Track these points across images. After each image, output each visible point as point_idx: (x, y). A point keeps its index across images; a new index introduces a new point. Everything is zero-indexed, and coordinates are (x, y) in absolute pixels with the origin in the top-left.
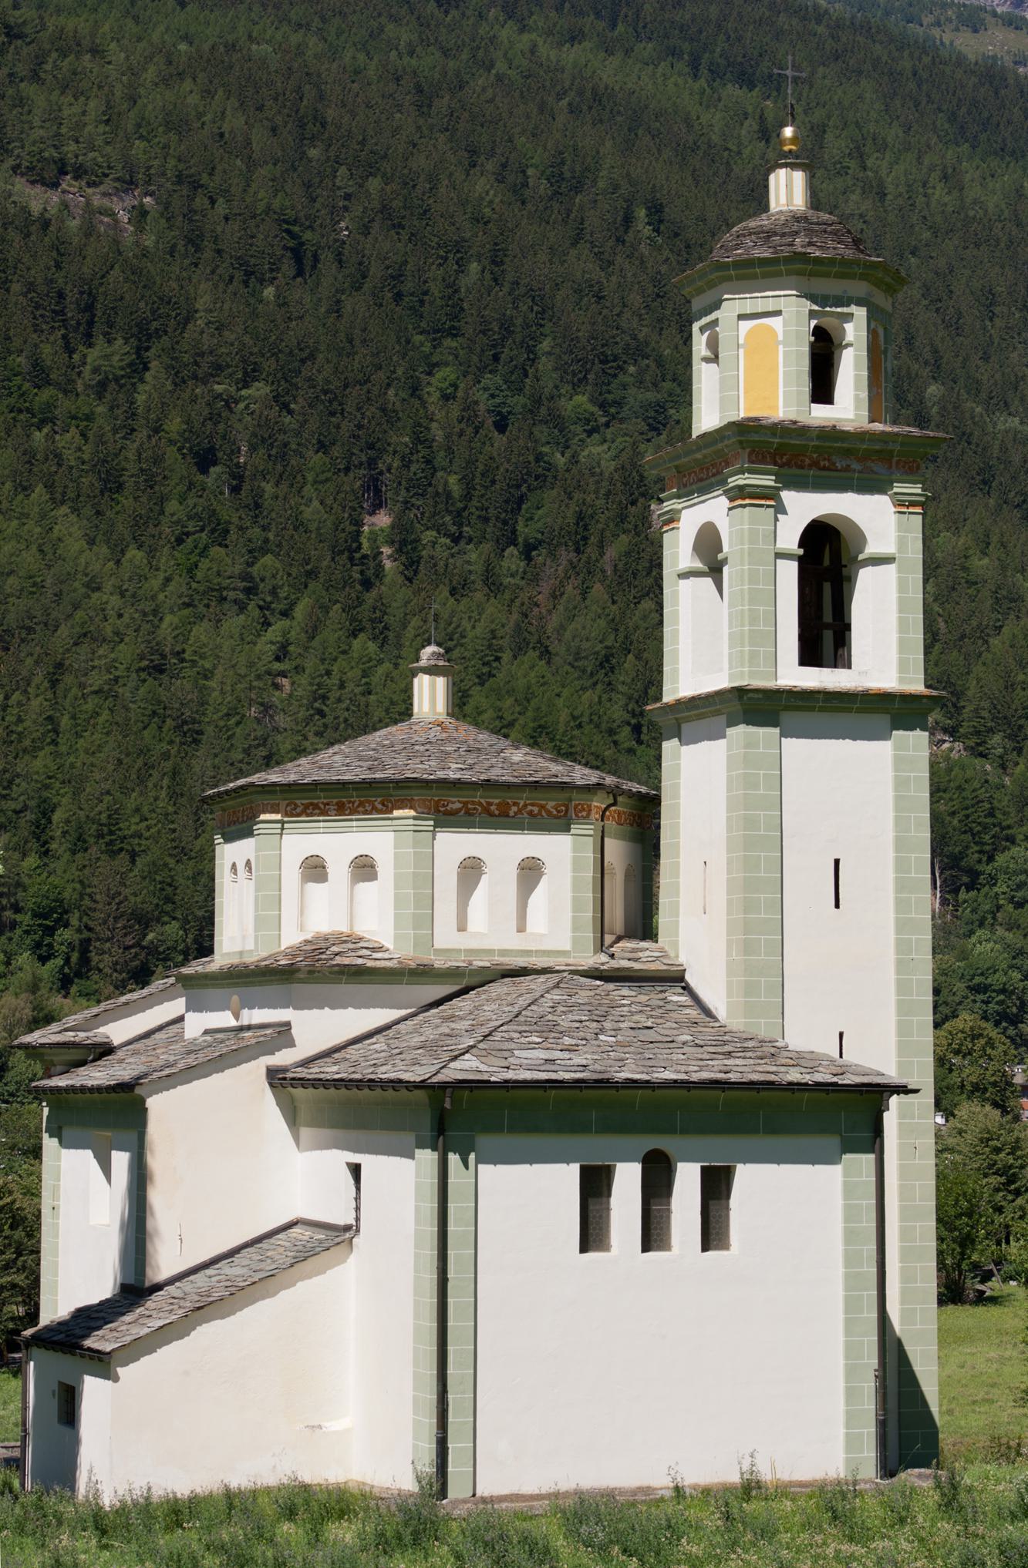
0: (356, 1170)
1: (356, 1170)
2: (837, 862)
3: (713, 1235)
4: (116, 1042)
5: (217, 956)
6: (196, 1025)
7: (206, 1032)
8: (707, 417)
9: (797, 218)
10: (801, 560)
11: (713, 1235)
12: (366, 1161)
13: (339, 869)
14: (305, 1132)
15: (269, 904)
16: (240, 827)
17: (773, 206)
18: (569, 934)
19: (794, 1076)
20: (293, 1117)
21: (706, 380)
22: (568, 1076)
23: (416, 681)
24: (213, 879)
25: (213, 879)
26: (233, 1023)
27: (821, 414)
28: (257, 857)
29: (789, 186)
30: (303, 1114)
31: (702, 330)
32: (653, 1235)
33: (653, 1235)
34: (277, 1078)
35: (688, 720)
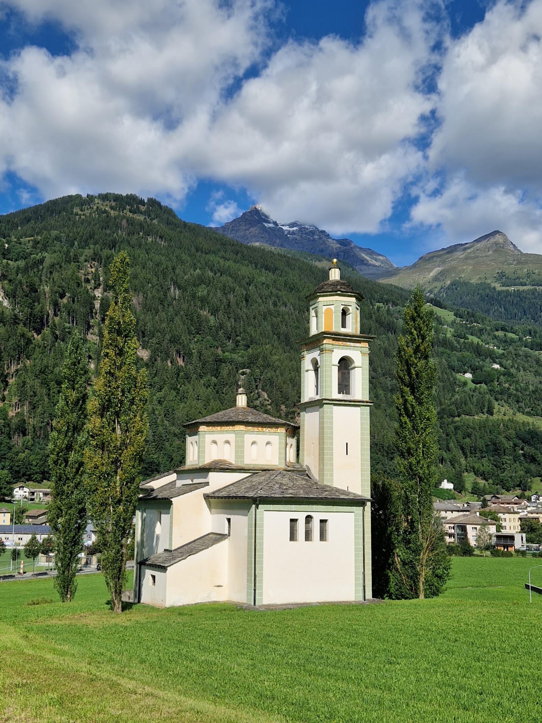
0: (229, 520)
1: (229, 520)
2: (347, 444)
3: (323, 537)
4: (155, 488)
5: (186, 466)
6: (179, 483)
7: (183, 485)
8: (314, 331)
9: (338, 282)
10: (339, 367)
11: (323, 537)
12: (232, 517)
13: (220, 442)
14: (213, 510)
15: (201, 452)
16: (195, 433)
17: (331, 279)
18: (278, 461)
19: (342, 497)
20: (210, 506)
21: (313, 321)
22: (288, 496)
23: (237, 397)
24: (300, 388)
25: (300, 388)
26: (191, 483)
27: (343, 331)
28: (199, 441)
29: (335, 273)
30: (212, 505)
31: (313, 309)
32: (308, 536)
33: (308, 536)
34: (207, 497)
35: (308, 407)
